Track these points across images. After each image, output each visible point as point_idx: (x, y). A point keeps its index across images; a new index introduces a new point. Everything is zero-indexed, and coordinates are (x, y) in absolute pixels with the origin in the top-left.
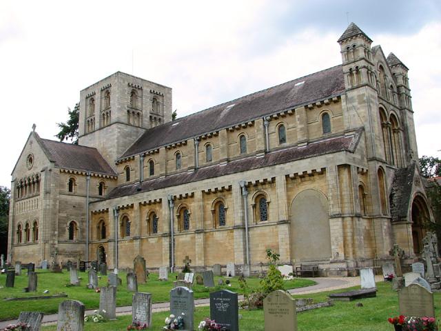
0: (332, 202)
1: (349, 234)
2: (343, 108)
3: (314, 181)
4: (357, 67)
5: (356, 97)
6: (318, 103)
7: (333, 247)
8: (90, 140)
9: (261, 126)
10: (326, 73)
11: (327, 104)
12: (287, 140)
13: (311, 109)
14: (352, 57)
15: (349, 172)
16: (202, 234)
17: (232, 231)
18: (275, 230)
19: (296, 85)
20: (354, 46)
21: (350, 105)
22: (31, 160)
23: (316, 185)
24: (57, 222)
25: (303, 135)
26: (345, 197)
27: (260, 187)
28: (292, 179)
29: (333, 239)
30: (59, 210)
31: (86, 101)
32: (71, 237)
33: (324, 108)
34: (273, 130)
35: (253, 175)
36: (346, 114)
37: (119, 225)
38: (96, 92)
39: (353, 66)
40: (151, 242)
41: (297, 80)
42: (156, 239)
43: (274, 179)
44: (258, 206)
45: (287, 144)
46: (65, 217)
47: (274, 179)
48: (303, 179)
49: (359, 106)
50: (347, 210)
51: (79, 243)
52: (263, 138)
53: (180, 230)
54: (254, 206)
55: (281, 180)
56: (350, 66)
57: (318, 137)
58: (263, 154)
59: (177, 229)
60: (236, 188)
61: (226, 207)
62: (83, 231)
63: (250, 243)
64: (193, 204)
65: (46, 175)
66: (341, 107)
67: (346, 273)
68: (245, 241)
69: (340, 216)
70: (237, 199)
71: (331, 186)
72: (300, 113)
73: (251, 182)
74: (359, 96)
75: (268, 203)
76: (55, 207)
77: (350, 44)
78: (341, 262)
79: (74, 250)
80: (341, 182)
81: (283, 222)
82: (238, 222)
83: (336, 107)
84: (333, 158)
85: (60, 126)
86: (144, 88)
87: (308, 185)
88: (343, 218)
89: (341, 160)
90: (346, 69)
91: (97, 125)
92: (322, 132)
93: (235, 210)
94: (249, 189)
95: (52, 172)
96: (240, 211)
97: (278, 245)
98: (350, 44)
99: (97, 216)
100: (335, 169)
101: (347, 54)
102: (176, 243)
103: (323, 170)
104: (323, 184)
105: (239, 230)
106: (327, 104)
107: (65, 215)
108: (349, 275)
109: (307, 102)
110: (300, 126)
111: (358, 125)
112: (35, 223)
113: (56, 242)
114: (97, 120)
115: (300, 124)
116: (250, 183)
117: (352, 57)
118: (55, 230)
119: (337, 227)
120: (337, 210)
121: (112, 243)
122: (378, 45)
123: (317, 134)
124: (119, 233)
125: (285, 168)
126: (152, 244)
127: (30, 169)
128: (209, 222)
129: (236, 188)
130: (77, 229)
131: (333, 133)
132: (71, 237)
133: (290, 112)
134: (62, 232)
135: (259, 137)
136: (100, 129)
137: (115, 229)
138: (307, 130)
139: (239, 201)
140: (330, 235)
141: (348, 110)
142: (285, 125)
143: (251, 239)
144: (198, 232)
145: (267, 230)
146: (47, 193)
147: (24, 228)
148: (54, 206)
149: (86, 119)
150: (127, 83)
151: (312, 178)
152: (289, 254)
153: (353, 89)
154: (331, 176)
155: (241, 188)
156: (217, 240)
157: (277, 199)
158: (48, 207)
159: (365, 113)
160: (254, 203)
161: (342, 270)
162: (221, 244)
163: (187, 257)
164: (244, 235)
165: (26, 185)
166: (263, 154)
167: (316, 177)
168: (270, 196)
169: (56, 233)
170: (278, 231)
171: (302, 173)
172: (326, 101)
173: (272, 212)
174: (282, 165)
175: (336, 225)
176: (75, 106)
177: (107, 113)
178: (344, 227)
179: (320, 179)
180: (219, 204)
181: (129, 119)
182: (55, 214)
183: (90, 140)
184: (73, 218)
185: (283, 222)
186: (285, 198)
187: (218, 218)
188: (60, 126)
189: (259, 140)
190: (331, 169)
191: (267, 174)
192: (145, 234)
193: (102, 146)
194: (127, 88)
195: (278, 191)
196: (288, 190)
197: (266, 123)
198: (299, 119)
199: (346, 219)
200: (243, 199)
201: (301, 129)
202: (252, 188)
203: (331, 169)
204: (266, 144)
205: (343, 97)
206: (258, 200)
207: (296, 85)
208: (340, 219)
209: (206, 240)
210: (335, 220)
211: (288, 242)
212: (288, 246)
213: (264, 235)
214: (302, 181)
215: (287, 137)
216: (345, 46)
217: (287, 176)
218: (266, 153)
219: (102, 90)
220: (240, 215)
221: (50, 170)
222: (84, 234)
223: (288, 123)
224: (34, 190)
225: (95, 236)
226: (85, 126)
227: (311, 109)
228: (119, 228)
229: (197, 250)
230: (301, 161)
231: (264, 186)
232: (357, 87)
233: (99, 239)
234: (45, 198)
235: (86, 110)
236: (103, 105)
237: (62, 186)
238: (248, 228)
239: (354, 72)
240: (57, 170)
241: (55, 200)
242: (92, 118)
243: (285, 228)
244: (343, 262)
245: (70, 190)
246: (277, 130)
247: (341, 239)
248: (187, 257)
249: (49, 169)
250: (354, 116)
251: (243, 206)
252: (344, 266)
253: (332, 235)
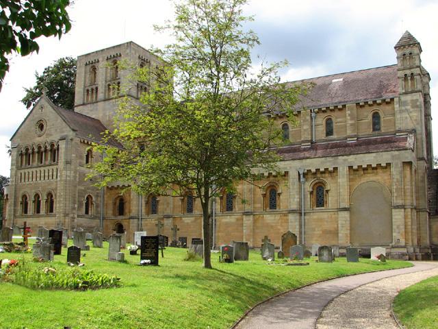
0: (395, 195)
1: (410, 223)
2: (396, 110)
3: (377, 174)
4: (412, 74)
5: (409, 102)
6: (370, 103)
7: (394, 234)
8: (91, 111)
9: (308, 118)
10: (365, 74)
11: (379, 104)
12: (334, 133)
13: (361, 106)
14: (408, 63)
15: (411, 169)
16: (252, 216)
17: (285, 215)
18: (333, 216)
19: (334, 81)
20: (411, 54)
21: (403, 108)
22: (41, 127)
23: (380, 177)
24: (77, 195)
25: (353, 131)
26: (408, 191)
27: (319, 175)
28: (355, 170)
29: (394, 227)
30: (79, 182)
31: (86, 68)
32: (87, 212)
33: (375, 108)
34: (320, 122)
35: (315, 163)
36: (398, 116)
37: (144, 203)
38: (100, 59)
39: (408, 72)
40: (186, 221)
41: (335, 76)
42: (193, 219)
43: (335, 169)
44: (315, 193)
45: (334, 136)
46: (84, 191)
47: (335, 169)
48: (365, 171)
49: (411, 110)
50: (408, 202)
51: (95, 218)
52: (310, 130)
53: (222, 211)
54: (311, 193)
55: (343, 170)
56: (405, 71)
57: (367, 133)
58: (310, 144)
59: (219, 210)
60: (293, 175)
61: (279, 191)
62: (97, 206)
63: (306, 227)
64: (240, 187)
65: (67, 144)
66: (394, 109)
67: (407, 257)
68: (301, 226)
69: (403, 207)
70: (293, 184)
71: (395, 180)
72: (350, 109)
73: (310, 170)
74: (412, 100)
75: (327, 191)
76: (75, 179)
77: (407, 51)
78: (402, 247)
79: (89, 225)
80: (405, 177)
81: (345, 209)
82: (294, 207)
83: (388, 108)
84: (399, 155)
85: (27, 91)
86: (152, 63)
87: (370, 177)
88: (254, 215)
89: (407, 158)
90: (401, 74)
91: (101, 95)
92: (372, 130)
93: (290, 195)
94: (306, 177)
95: (73, 142)
96: (297, 196)
97: (338, 230)
98: (407, 51)
99: (113, 192)
100: (400, 165)
101: (403, 60)
102: (218, 223)
103: (388, 165)
104: (386, 178)
105: (295, 214)
106: (379, 104)
107: (83, 188)
108: (410, 259)
109: (346, 102)
110: (350, 122)
111: (410, 126)
112: (50, 195)
113: (76, 216)
114: (101, 90)
115: (351, 119)
116: (309, 171)
117: (408, 63)
118: (74, 203)
119: (396, 217)
120: (400, 202)
121: (136, 220)
122: (49, 37)
123: (366, 130)
124: (143, 211)
125: (349, 160)
126: (188, 223)
127: (40, 136)
128: (258, 205)
129: (293, 175)
130: (92, 204)
131: (383, 131)
132: (87, 212)
133: (340, 107)
134: (80, 205)
135: (305, 127)
136: (105, 100)
137: (138, 206)
138: (356, 126)
139: (296, 186)
140: (392, 224)
141: (401, 112)
142: (333, 119)
143: (306, 224)
144: (247, 214)
145: (325, 215)
146: (68, 163)
147: (33, 199)
148: (75, 177)
149: (85, 87)
150: (138, 55)
151: (375, 171)
152: (349, 239)
153: (406, 93)
154: (395, 171)
155: (299, 175)
156: (268, 224)
157: (339, 189)
158: (68, 178)
159: (417, 117)
160: (311, 190)
161: (403, 255)
162: (272, 227)
163: (266, 237)
164: (300, 219)
165: (33, 153)
166: (310, 144)
167: (379, 171)
168: (330, 184)
169: (76, 206)
170: (338, 218)
171: (366, 166)
172: (379, 101)
173: (331, 200)
174: (345, 157)
175: (398, 216)
176: (44, 70)
177: (92, 89)
178: (405, 217)
179: (384, 172)
180: (271, 188)
181: (137, 93)
182: (76, 186)
183: (91, 111)
184: (90, 192)
185: (345, 209)
186: (347, 187)
187: (186, 205)
188: (27, 91)
189: (305, 130)
190: (397, 165)
191: (328, 164)
192: (178, 213)
193: (108, 118)
194: (137, 61)
195: (339, 180)
196: (351, 180)
197: (313, 115)
198: (349, 115)
199: (407, 210)
200: (300, 186)
201: (351, 125)
202: (310, 176)
203: (397, 165)
204: (312, 135)
205: (396, 100)
206: (315, 188)
207: (334, 81)
208: (403, 210)
209: (255, 221)
210: (397, 210)
211: (349, 228)
212: (349, 231)
213: (321, 220)
214: (364, 173)
215: (334, 130)
216: (401, 52)
217: (350, 168)
218: (312, 143)
219: (86, 64)
220: (297, 200)
221: (72, 140)
222: (99, 209)
223: (337, 119)
224: (46, 159)
225: (110, 212)
226: (84, 95)
227: (361, 106)
228: (144, 205)
229: (244, 231)
230: (366, 155)
231: (323, 175)
232: (412, 92)
233: (114, 215)
234: (65, 169)
235: (85, 77)
236: (87, 80)
237: (81, 157)
238: (305, 213)
239: (409, 78)
240: (77, 140)
241: (75, 172)
242: (94, 87)
243: (346, 214)
244: (405, 247)
245: (87, 162)
246: (324, 123)
247: (402, 227)
248: (266, 237)
249: (70, 138)
250: (406, 118)
251: (300, 192)
252: (404, 251)
253: (394, 223)
